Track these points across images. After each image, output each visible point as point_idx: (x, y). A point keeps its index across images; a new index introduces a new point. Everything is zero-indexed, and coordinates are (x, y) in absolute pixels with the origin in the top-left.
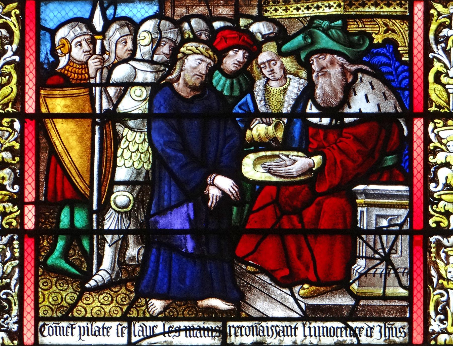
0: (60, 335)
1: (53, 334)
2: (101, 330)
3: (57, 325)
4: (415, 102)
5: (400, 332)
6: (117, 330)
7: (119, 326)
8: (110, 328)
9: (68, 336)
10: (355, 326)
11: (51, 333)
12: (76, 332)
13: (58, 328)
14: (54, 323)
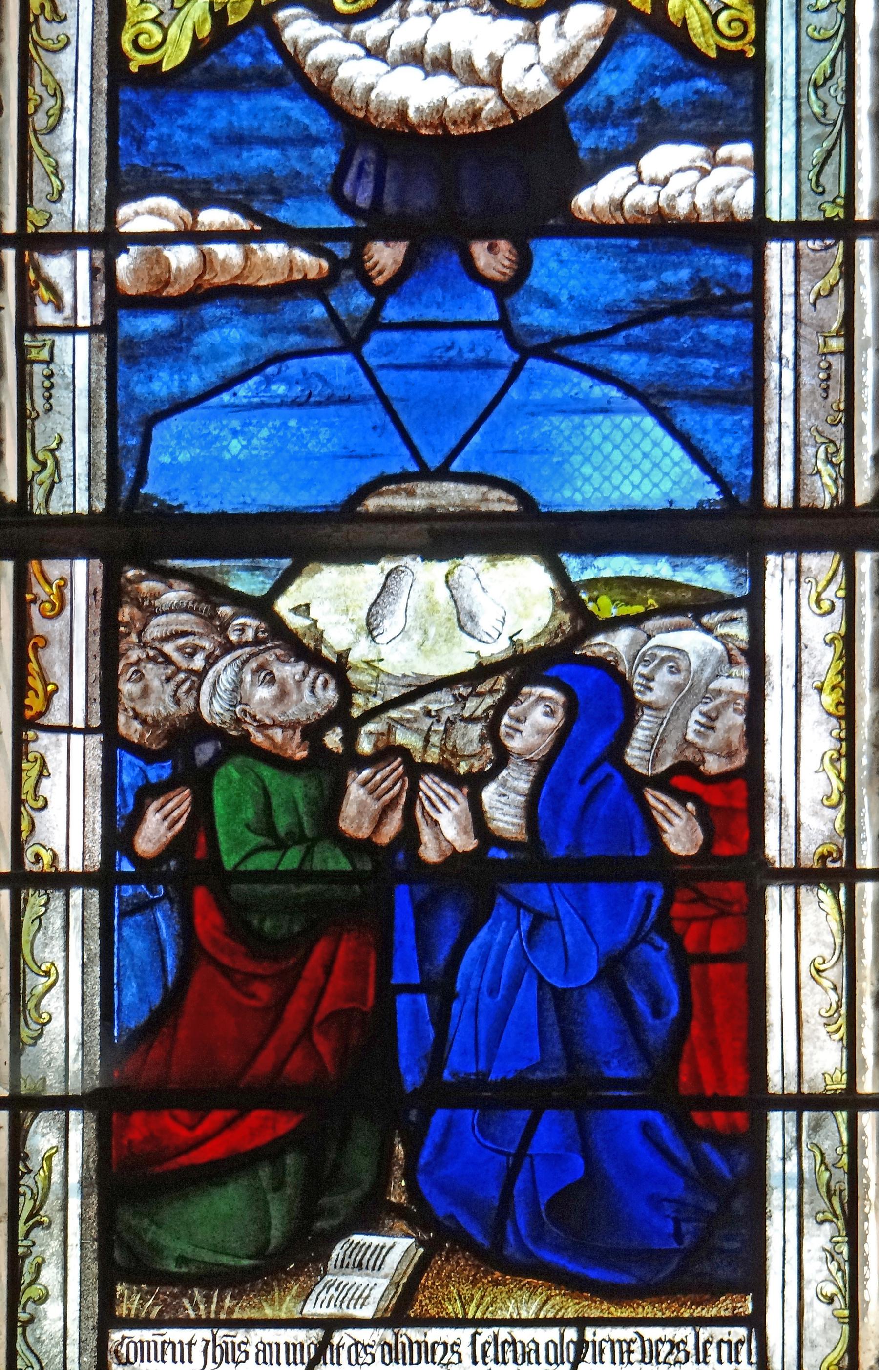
5: (453, 1352)
8: (711, 1343)
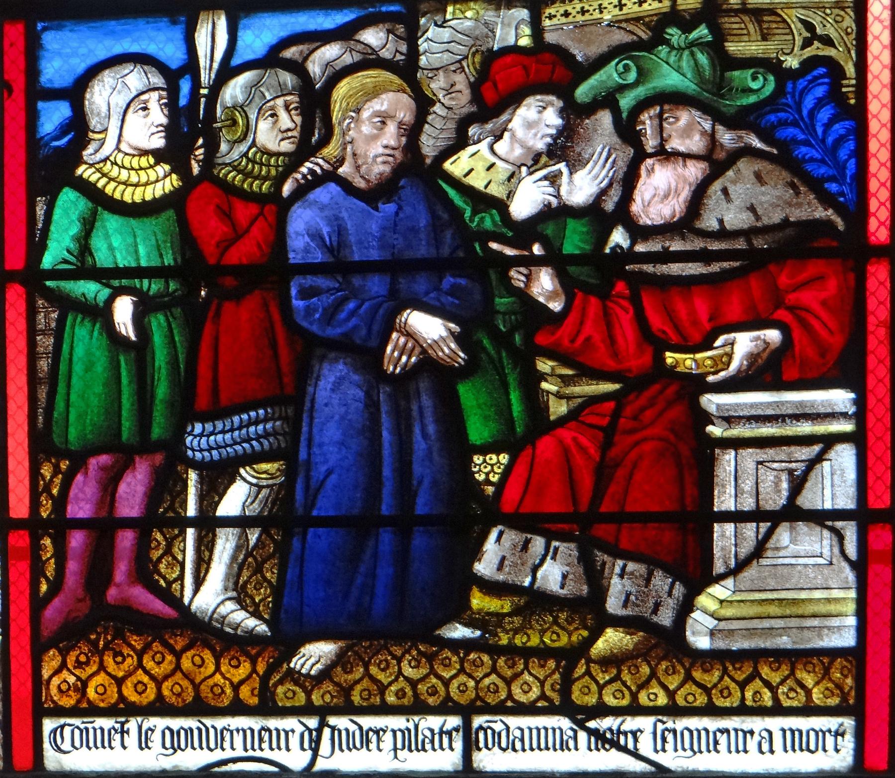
0: (104, 747)
1: (187, 746)
2: (437, 737)
3: (89, 726)
4: (22, 306)
6: (655, 734)
7: (659, 725)
8: (153, 731)
9: (112, 748)
10: (809, 728)
11: (77, 744)
12: (132, 740)
13: (91, 732)
14: (83, 723)
